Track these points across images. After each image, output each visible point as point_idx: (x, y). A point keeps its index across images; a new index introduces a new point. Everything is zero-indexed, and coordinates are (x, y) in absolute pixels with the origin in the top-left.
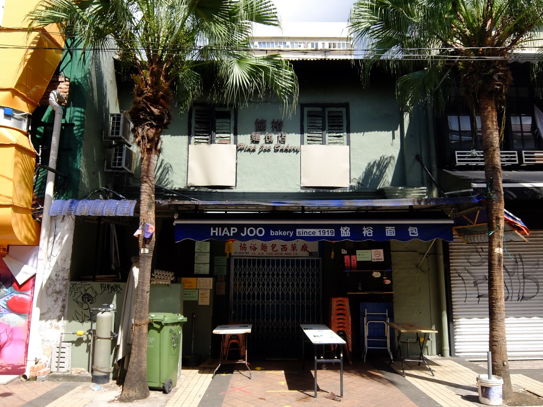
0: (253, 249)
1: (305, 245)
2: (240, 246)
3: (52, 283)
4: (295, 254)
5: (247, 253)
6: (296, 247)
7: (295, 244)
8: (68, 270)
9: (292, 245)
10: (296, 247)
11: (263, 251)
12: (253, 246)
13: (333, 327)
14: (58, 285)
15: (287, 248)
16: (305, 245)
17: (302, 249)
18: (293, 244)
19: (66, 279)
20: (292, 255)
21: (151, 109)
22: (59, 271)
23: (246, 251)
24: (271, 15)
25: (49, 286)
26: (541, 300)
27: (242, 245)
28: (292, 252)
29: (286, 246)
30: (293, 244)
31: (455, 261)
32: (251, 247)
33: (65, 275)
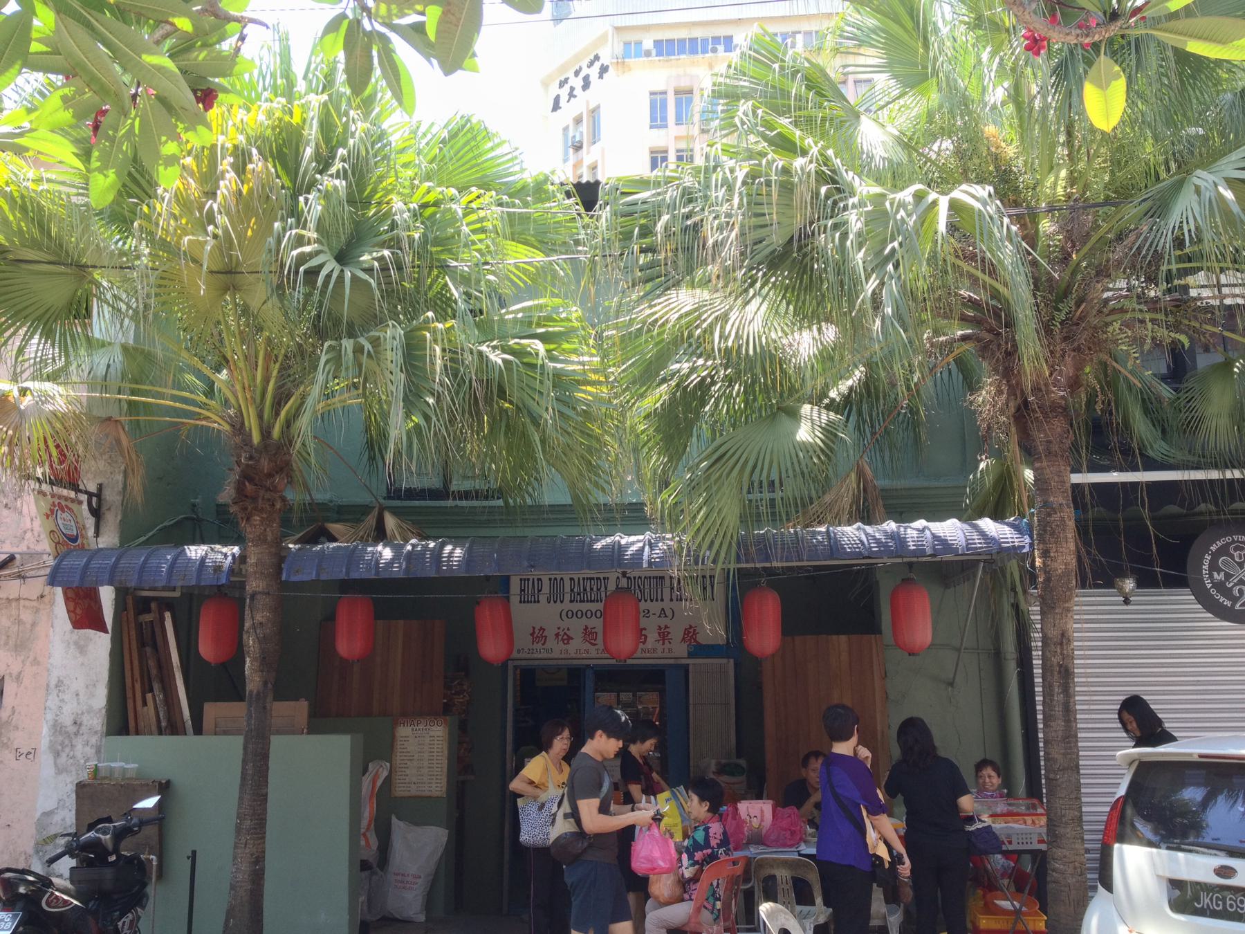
0: (563, 640)
1: (691, 627)
2: (532, 634)
3: (67, 742)
4: (667, 651)
5: (547, 651)
6: (669, 633)
7: (666, 627)
8: (100, 710)
9: (660, 628)
10: (669, 633)
11: (587, 646)
12: (562, 633)
13: (780, 896)
14: (79, 747)
15: (646, 637)
16: (691, 627)
17: (684, 638)
18: (663, 626)
19: (96, 732)
20: (659, 654)
21: (197, 167)
22: (83, 713)
23: (545, 646)
24: (555, 516)
25: (60, 748)
26: (4, 272)
27: (537, 631)
28: (659, 646)
29: (644, 632)
30: (663, 626)
31: (17, 294)
32: (557, 635)
33: (95, 722)
